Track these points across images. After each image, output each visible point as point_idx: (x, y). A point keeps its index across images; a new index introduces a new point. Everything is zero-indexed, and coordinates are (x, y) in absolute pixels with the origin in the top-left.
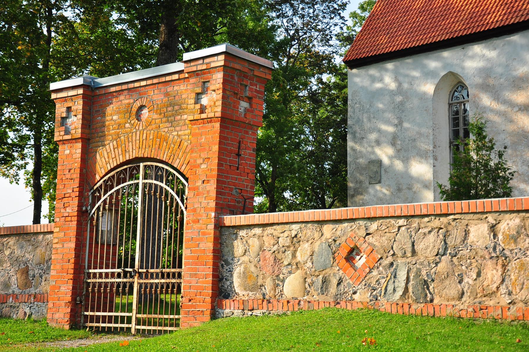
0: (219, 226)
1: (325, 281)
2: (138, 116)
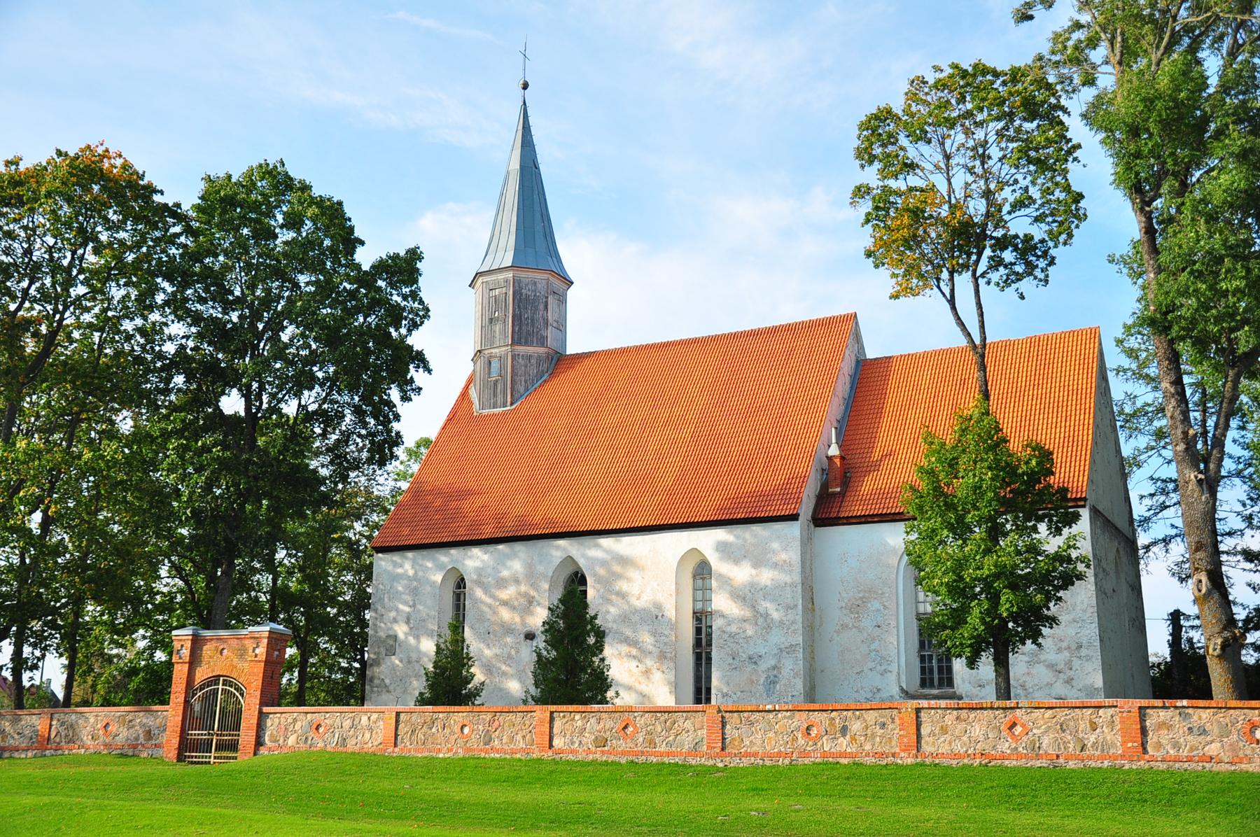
0: (260, 712)
1: (306, 738)
2: (221, 653)
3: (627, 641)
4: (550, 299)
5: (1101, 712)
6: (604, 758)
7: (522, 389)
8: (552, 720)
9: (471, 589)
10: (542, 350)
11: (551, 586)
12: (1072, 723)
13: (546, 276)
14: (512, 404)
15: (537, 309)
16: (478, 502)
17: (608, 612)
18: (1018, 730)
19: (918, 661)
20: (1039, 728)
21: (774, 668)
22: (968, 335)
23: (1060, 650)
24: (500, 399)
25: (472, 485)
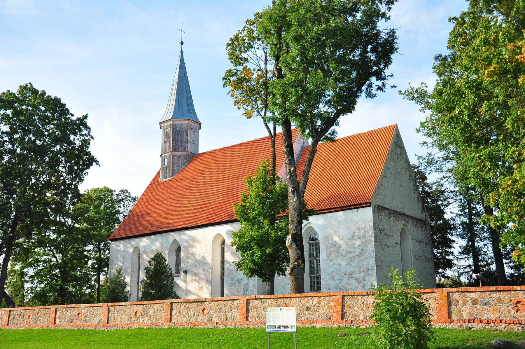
3: (196, 274)
4: (189, 131)
5: (235, 302)
6: (70, 328)
7: (176, 170)
8: (56, 312)
9: (142, 255)
10: (185, 153)
11: (169, 252)
12: (224, 308)
13: (187, 122)
14: (172, 177)
15: (183, 136)
16: (148, 218)
17: (188, 262)
18: (205, 312)
19: (309, 279)
20: (212, 310)
21: (247, 284)
22: (270, 132)
23: (360, 272)
24: (168, 175)
25: (150, 211)
